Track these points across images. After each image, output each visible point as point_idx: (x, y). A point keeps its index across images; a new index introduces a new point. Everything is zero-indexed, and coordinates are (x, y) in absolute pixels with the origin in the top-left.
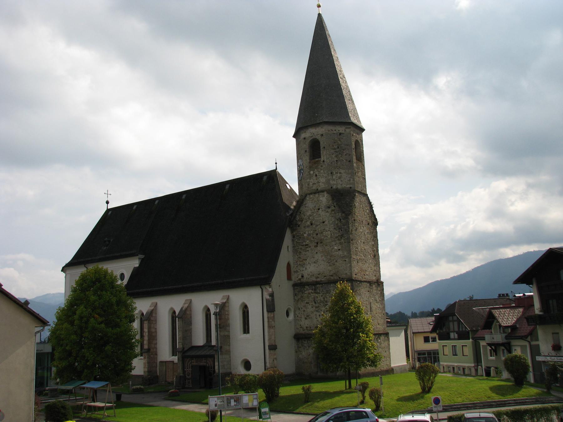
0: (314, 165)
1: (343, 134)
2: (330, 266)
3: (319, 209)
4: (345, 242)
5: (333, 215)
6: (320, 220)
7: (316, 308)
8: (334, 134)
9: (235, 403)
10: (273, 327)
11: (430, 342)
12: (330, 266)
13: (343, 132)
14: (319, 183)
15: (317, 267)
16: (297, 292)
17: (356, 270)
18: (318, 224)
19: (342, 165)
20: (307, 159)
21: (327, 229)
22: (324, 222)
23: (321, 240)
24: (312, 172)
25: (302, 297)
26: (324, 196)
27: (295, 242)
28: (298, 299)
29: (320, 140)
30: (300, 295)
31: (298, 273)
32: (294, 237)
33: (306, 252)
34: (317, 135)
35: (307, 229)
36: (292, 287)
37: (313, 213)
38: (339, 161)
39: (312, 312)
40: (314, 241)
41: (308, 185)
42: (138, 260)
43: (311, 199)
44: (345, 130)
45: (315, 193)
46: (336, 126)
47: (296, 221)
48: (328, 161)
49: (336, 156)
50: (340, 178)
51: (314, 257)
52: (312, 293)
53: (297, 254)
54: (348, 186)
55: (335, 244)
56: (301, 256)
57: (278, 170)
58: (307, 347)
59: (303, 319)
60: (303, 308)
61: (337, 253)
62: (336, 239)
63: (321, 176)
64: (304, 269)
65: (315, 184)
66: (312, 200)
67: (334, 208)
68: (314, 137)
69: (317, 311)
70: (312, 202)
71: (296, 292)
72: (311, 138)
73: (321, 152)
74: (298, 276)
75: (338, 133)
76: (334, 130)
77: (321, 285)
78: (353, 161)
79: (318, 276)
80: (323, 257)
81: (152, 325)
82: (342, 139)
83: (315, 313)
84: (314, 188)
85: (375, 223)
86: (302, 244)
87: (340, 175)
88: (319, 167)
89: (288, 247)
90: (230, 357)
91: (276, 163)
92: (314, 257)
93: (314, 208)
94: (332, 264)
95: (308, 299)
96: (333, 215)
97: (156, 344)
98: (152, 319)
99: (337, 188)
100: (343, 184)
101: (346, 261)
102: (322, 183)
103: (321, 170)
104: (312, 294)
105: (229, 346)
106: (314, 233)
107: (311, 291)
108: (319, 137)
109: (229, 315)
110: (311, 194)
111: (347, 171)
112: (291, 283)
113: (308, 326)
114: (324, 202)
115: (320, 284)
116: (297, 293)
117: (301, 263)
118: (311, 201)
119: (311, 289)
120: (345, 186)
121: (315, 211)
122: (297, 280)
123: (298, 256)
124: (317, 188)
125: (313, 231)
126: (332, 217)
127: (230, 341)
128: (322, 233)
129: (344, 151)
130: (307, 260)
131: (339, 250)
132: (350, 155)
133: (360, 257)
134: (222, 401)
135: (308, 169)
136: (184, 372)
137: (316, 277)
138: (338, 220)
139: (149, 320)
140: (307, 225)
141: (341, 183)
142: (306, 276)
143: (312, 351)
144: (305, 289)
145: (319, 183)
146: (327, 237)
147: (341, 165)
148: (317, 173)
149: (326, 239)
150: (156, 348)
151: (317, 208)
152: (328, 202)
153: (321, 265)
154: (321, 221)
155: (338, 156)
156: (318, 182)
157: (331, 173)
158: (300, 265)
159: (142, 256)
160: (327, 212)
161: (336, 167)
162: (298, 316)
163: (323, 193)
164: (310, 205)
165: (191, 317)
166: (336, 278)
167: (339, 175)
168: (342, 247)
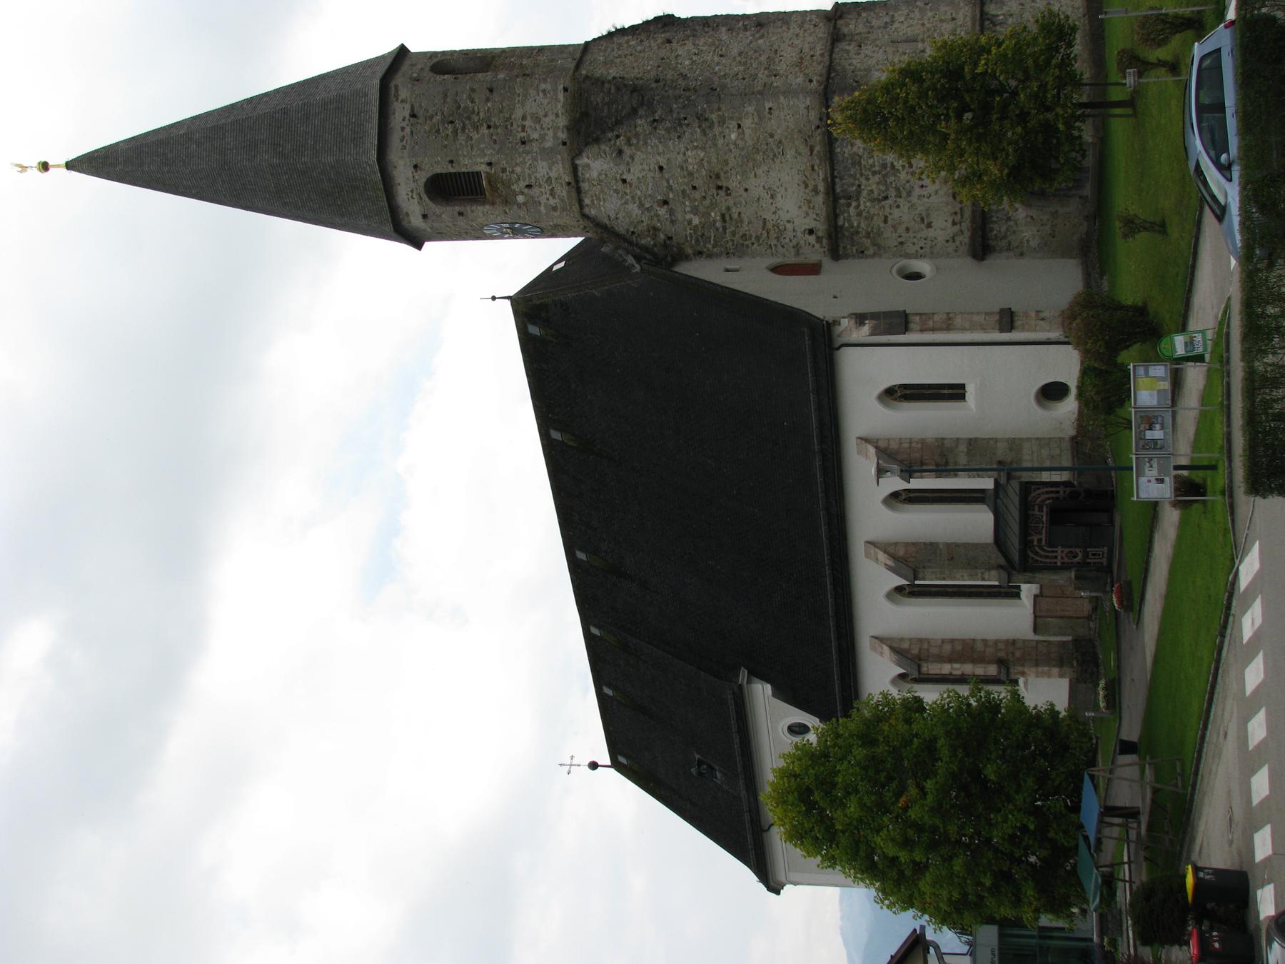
1: (412, 107)
3: (624, 181)
4: (719, 109)
6: (653, 178)
7: (901, 197)
8: (412, 133)
9: (1158, 426)
10: (949, 319)
13: (408, 106)
15: (786, 190)
18: (665, 184)
19: (501, 112)
21: (680, 158)
22: (661, 168)
23: (711, 177)
25: (868, 235)
26: (588, 166)
27: (715, 250)
28: (875, 245)
29: (429, 174)
30: (864, 239)
31: (802, 243)
32: (700, 253)
33: (742, 221)
35: (679, 216)
37: (633, 198)
38: (491, 121)
39: (912, 207)
40: (713, 196)
41: (555, 209)
42: (753, 685)
43: (595, 202)
45: (579, 191)
47: (655, 245)
48: (491, 151)
49: (477, 128)
50: (538, 120)
51: (758, 199)
52: (858, 206)
53: (747, 246)
54: (561, 96)
55: (724, 137)
56: (754, 235)
59: (931, 233)
61: (747, 132)
62: (710, 135)
64: (789, 226)
65: (552, 190)
66: (599, 199)
68: (422, 190)
69: (909, 194)
72: (425, 197)
73: (464, 170)
75: (409, 120)
76: (401, 134)
77: (837, 180)
79: (810, 187)
80: (759, 172)
81: (934, 651)
82: (427, 110)
83: (914, 199)
84: (564, 193)
85: (666, 23)
86: (721, 230)
87: (528, 118)
89: (727, 270)
90: (1029, 439)
91: (494, 298)
92: (758, 199)
93: (620, 195)
96: (641, 142)
97: (985, 641)
98: (915, 651)
99: (565, 130)
100: (555, 111)
101: (770, 109)
102: (550, 169)
103: (513, 172)
104: (862, 207)
105: (996, 440)
106: (689, 197)
107: (852, 210)
108: (422, 177)
109: (911, 439)
110: (580, 201)
111: (517, 99)
112: (827, 263)
113: (950, 220)
114: (605, 166)
115: (833, 183)
116: (857, 250)
117: (773, 235)
119: (846, 208)
120: (559, 106)
121: (628, 191)
122: (821, 247)
123: (753, 244)
124: (564, 183)
125: (684, 198)
126: (646, 143)
128: (691, 174)
130: (765, 219)
131: (739, 126)
134: (1148, 464)
136: (1065, 567)
137: (813, 193)
138: (655, 128)
139: (920, 660)
141: (551, 117)
142: (809, 223)
144: (847, 225)
148: (522, 184)
150: (996, 642)
153: (780, 180)
154: (658, 175)
157: (523, 143)
158: (777, 238)
159: (743, 675)
160: (633, 159)
161: (506, 127)
162: (922, 248)
163: (580, 169)
164: (612, 206)
167: (528, 123)
168: (731, 118)
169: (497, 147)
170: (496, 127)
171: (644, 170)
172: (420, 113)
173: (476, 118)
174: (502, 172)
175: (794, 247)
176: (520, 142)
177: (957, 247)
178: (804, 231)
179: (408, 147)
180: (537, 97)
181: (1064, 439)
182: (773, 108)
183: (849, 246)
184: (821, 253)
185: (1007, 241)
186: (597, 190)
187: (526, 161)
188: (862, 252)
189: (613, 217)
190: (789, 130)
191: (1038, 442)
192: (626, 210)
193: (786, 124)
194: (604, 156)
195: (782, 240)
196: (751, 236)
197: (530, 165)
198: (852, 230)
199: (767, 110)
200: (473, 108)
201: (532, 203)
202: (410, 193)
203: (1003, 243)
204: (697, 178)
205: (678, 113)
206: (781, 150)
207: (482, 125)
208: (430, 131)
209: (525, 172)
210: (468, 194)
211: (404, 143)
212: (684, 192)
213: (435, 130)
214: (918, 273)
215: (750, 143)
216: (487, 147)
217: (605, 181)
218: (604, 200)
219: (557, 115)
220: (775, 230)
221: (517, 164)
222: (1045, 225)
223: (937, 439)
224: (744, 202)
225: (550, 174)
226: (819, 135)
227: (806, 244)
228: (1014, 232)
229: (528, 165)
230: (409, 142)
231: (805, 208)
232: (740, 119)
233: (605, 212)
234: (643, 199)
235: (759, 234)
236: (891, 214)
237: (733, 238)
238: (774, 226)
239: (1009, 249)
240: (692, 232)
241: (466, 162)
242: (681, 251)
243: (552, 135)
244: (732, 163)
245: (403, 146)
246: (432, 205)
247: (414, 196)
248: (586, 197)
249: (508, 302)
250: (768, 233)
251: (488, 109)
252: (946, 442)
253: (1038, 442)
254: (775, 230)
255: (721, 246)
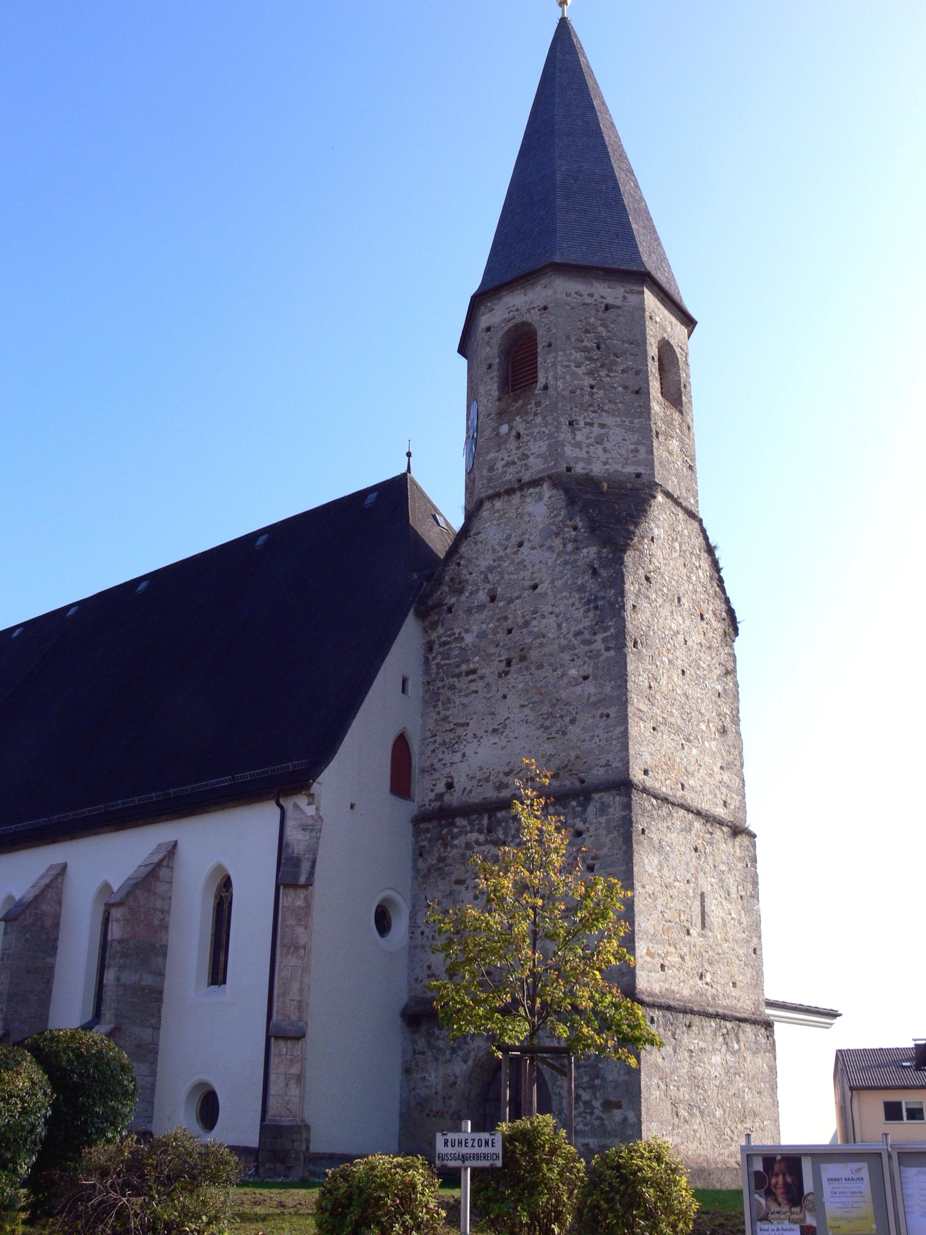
0: (514, 404)
1: (618, 307)
2: (549, 739)
3: (520, 545)
5: (567, 557)
6: (524, 579)
10: (297, 948)
11: (902, 1119)
12: (549, 739)
13: (618, 302)
14: (527, 456)
15: (503, 748)
16: (425, 843)
17: (646, 756)
20: (490, 390)
22: (535, 587)
24: (504, 429)
25: (442, 859)
28: (429, 870)
29: (536, 325)
31: (437, 775)
32: (430, 647)
34: (529, 311)
36: (411, 825)
37: (500, 558)
38: (599, 389)
40: (500, 656)
41: (491, 469)
43: (497, 515)
44: (625, 297)
45: (510, 492)
46: (596, 284)
48: (561, 386)
49: (590, 373)
50: (599, 441)
51: (493, 714)
52: (477, 843)
53: (435, 706)
54: (630, 469)
55: (573, 660)
56: (448, 713)
57: (414, 474)
58: (448, 1052)
60: (445, 900)
61: (578, 689)
63: (535, 434)
65: (514, 463)
66: (501, 517)
67: (574, 533)
68: (518, 320)
70: (499, 525)
71: (423, 844)
72: (510, 325)
73: (540, 359)
74: (434, 785)
75: (602, 303)
76: (585, 293)
78: (648, 393)
80: (527, 711)
82: (613, 322)
86: (457, 671)
87: (602, 431)
88: (529, 407)
89: (405, 681)
90: (153, 1073)
91: (409, 455)
92: (493, 714)
93: (504, 542)
94: (557, 732)
95: (463, 868)
96: (567, 557)
100: (610, 461)
101: (608, 716)
102: (538, 456)
103: (536, 414)
104: (477, 849)
105: (156, 1028)
106: (499, 626)
107: (474, 836)
108: (534, 317)
109: (169, 912)
110: (497, 495)
111: (627, 420)
112: (409, 809)
114: (539, 519)
116: (424, 847)
117: (448, 737)
118: (495, 522)
119: (476, 828)
120: (618, 467)
121: (509, 551)
122: (430, 801)
123: (439, 713)
124: (520, 474)
125: (499, 620)
126: (566, 563)
127: (159, 1011)
128: (527, 624)
129: (619, 360)
130: (468, 724)
131: (585, 678)
132: (637, 373)
133: (665, 716)
135: (492, 419)
137: (497, 784)
140: (476, 601)
141: (603, 457)
142: (461, 782)
143: (465, 1067)
144: (455, 830)
145: (527, 456)
146: (544, 636)
147: (606, 401)
149: (541, 644)
151: (514, 540)
152: (555, 516)
153: (516, 738)
154: (528, 583)
155: (598, 371)
156: (524, 454)
157: (571, 423)
158: (444, 743)
161: (590, 406)
162: (422, 933)
164: (491, 535)
165: (57, 925)
166: (567, 783)
167: (596, 430)
168: (596, 667)
169: (566, 393)
170: (592, 395)
171: (533, 566)
172: (611, 315)
173: (602, 373)
174: (535, 403)
175: (432, 765)
176: (573, 419)
177: (422, 981)
178: (451, 777)
179: (569, 299)
180: (629, 442)
181: (151, 1122)
182: (609, 720)
183: (429, 835)
184: (423, 800)
185: (426, 1050)
186: (512, 514)
187: (549, 427)
188: (421, 855)
189: (479, 538)
190: (579, 744)
191: (149, 1086)
192: (486, 552)
193: (587, 738)
194: (552, 515)
195: (441, 749)
196: (448, 709)
197: (544, 432)
198: (449, 838)
199: (605, 711)
200: (615, 371)
201: (499, 441)
202: (515, 308)
203: (422, 1043)
204: (521, 633)
205: (603, 598)
206: (554, 735)
207: (594, 379)
208: (588, 324)
209: (536, 427)
210: (513, 377)
211: (573, 295)
212: (506, 618)
213: (588, 328)
214: (390, 928)
215: (564, 695)
216: (566, 383)
217: (521, 522)
218: (499, 525)
219: (605, 463)
220: (454, 739)
221: (545, 417)
222: (444, 1103)
223: (165, 947)
224: (490, 695)
225: (532, 457)
226: (572, 783)
227: (435, 780)
228: (436, 1059)
229: (544, 429)
230: (575, 300)
231: (479, 775)
232: (596, 678)
233: (485, 528)
234: (499, 570)
235: (451, 719)
236: (467, 888)
237: (446, 688)
238: (459, 737)
239: (415, 1052)
240: (457, 636)
241: (548, 361)
242: (434, 626)
243: (581, 456)
244: (540, 674)
245: (570, 294)
246: (501, 333)
247: (511, 313)
248: (504, 502)
249: (402, 469)
250: (451, 731)
251: (614, 387)
252: (160, 959)
253: (149, 1086)
254: (454, 739)
255: (438, 673)
